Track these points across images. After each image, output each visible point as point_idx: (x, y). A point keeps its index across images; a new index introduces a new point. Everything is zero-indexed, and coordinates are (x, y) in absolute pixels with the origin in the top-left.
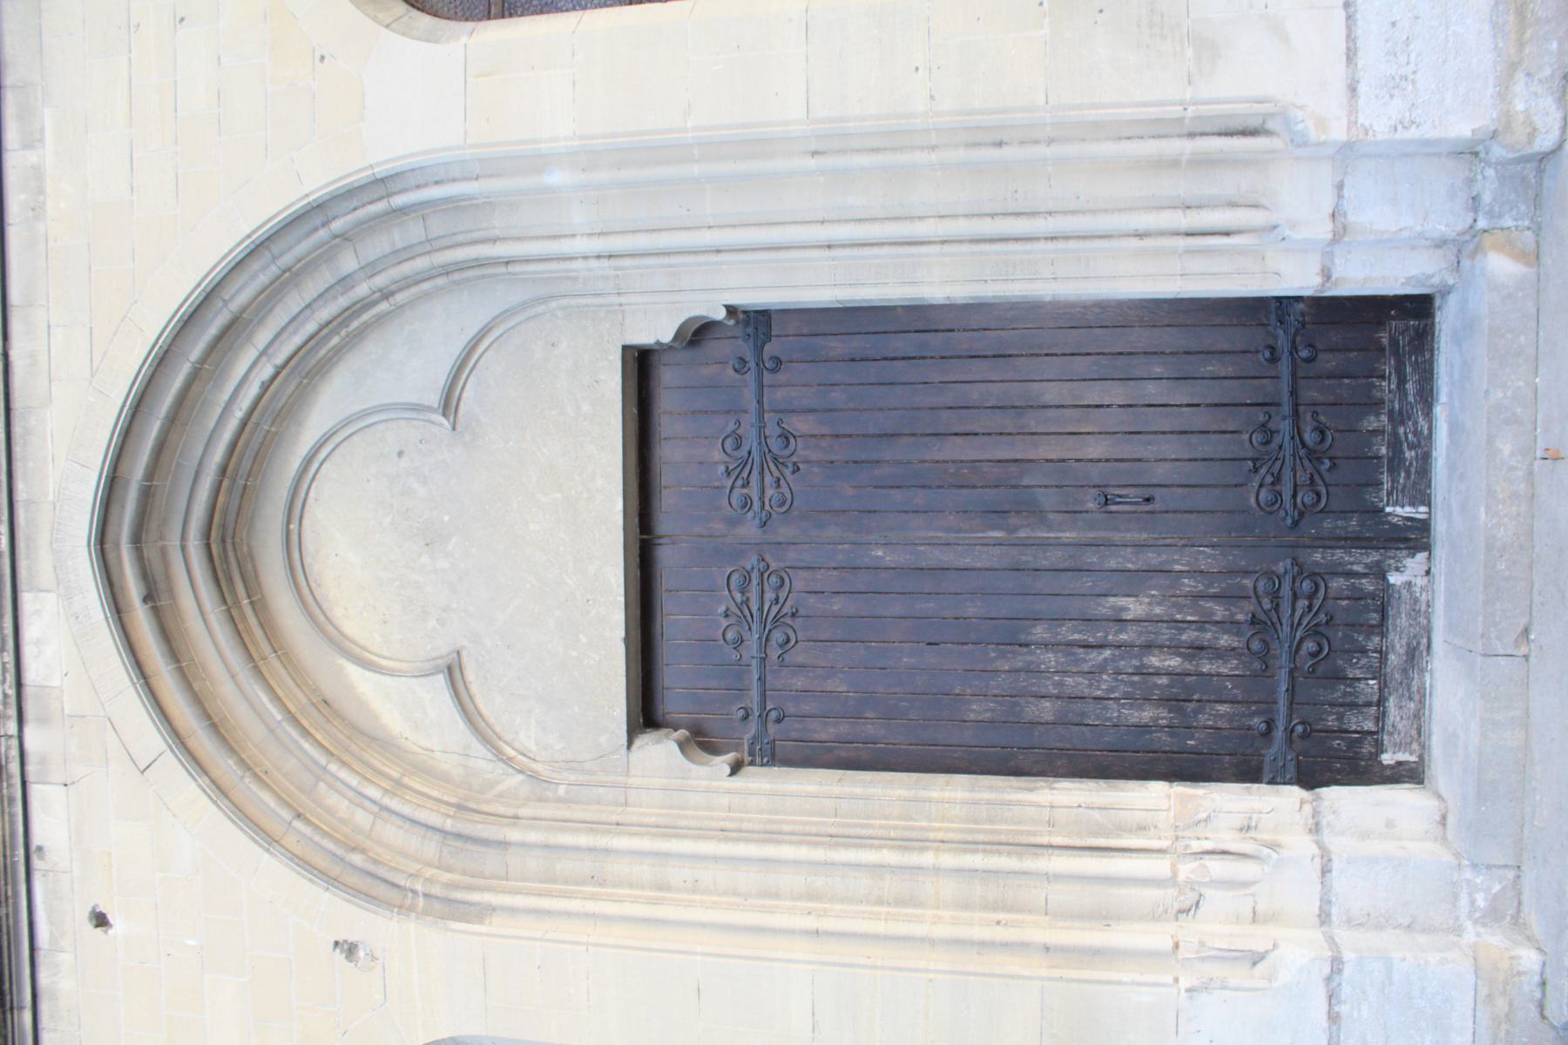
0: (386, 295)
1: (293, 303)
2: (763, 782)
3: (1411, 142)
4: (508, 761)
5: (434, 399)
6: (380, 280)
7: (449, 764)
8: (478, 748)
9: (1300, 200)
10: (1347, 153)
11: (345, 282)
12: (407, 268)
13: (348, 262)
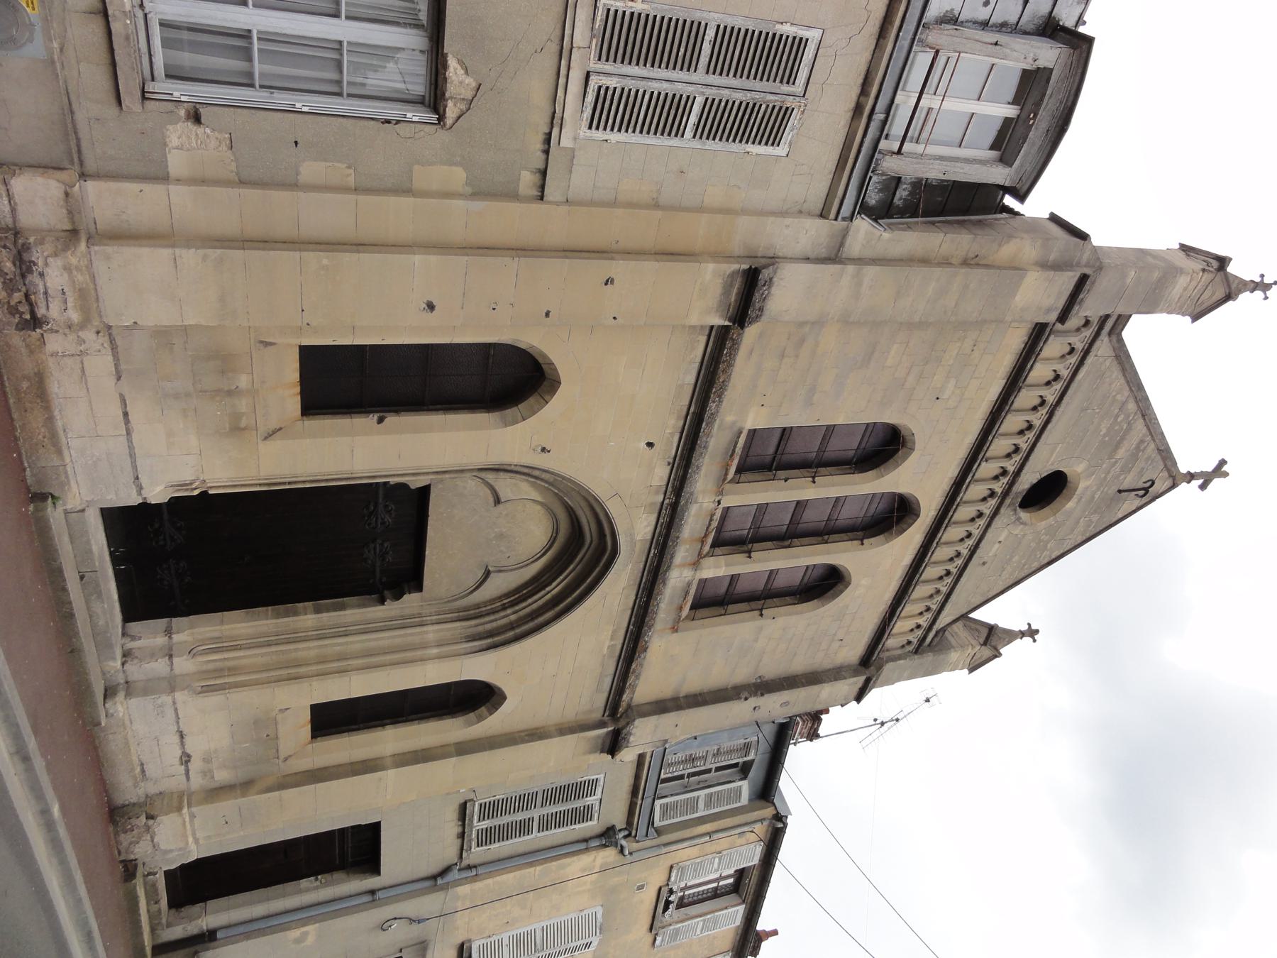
0: (504, 608)
13: (513, 617)
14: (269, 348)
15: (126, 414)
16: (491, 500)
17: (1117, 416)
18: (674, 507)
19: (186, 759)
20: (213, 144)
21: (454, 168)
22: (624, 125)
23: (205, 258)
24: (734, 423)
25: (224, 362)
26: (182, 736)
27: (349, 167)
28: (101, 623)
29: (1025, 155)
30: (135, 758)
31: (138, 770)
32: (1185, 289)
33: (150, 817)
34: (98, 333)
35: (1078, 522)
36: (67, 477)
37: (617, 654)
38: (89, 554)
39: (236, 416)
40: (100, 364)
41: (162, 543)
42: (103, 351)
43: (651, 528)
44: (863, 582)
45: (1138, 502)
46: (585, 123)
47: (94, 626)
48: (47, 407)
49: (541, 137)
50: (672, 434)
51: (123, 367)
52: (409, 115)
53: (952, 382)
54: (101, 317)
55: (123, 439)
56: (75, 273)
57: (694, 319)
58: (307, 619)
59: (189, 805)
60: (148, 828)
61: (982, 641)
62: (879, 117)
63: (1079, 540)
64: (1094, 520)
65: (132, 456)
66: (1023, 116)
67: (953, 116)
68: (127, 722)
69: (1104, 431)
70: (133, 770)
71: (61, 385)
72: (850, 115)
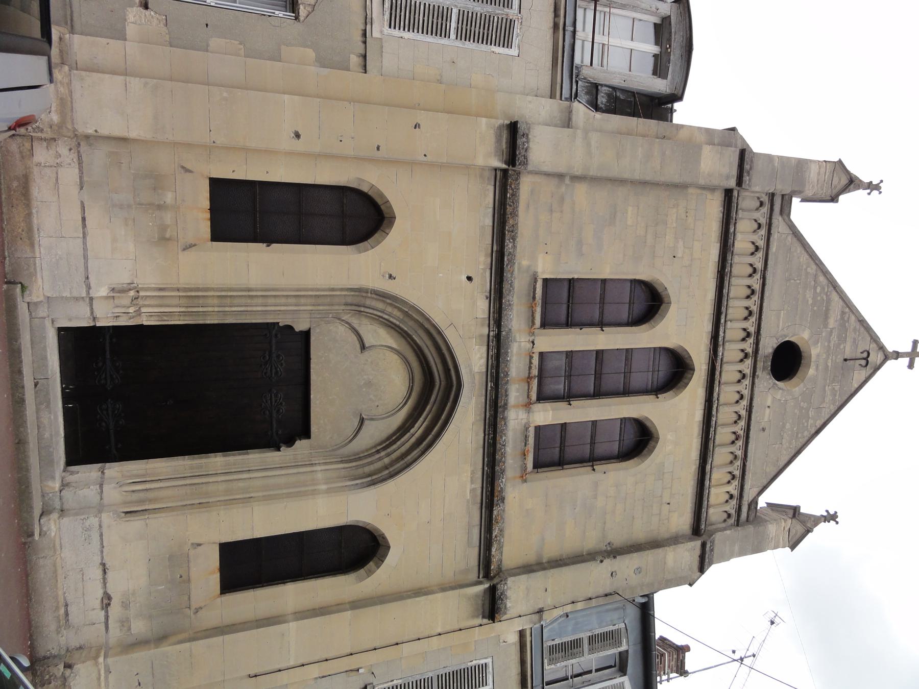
0: (378, 452)
1: (403, 449)
2: (270, 319)
3: (83, 514)
4: (347, 323)
5: (366, 422)
6: (377, 456)
7: (365, 321)
8: (356, 326)
9: (112, 494)
10: (100, 509)
11: (388, 455)
12: (369, 460)
13: (387, 461)
14: (188, 174)
15: (84, 219)
16: (358, 346)
17: (815, 288)
18: (498, 336)
19: (107, 601)
20: (155, 22)
21: (308, 50)
22: (411, 26)
23: (146, 84)
24: (529, 267)
25: (156, 180)
26: (105, 572)
27: (241, 44)
28: (47, 435)
29: (673, 71)
30: (60, 593)
31: (62, 611)
32: (819, 174)
33: (68, 666)
34: (70, 150)
35: (825, 390)
36: (35, 269)
37: (479, 501)
38: (45, 364)
39: (163, 228)
40: (70, 175)
41: (103, 382)
42: (73, 164)
43: (484, 361)
44: (669, 437)
45: (864, 374)
46: (386, 24)
47: (40, 438)
48: (28, 205)
49: (360, 33)
50: (484, 270)
51: (85, 179)
52: (277, 12)
53: (681, 243)
54: (73, 124)
55: (80, 241)
56: (59, 85)
57: (480, 161)
58: (217, 461)
59: (105, 657)
60: (65, 679)
61: (791, 516)
62: (570, 28)
63: (833, 410)
64: (837, 388)
65: (85, 257)
66: (664, 50)
67: (621, 50)
68: (58, 547)
69: (810, 302)
70: (57, 608)
71: (40, 191)
72: (552, 30)
